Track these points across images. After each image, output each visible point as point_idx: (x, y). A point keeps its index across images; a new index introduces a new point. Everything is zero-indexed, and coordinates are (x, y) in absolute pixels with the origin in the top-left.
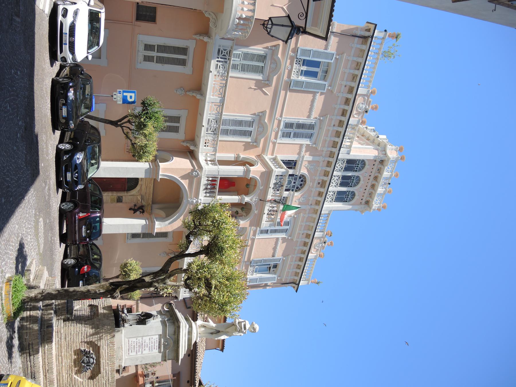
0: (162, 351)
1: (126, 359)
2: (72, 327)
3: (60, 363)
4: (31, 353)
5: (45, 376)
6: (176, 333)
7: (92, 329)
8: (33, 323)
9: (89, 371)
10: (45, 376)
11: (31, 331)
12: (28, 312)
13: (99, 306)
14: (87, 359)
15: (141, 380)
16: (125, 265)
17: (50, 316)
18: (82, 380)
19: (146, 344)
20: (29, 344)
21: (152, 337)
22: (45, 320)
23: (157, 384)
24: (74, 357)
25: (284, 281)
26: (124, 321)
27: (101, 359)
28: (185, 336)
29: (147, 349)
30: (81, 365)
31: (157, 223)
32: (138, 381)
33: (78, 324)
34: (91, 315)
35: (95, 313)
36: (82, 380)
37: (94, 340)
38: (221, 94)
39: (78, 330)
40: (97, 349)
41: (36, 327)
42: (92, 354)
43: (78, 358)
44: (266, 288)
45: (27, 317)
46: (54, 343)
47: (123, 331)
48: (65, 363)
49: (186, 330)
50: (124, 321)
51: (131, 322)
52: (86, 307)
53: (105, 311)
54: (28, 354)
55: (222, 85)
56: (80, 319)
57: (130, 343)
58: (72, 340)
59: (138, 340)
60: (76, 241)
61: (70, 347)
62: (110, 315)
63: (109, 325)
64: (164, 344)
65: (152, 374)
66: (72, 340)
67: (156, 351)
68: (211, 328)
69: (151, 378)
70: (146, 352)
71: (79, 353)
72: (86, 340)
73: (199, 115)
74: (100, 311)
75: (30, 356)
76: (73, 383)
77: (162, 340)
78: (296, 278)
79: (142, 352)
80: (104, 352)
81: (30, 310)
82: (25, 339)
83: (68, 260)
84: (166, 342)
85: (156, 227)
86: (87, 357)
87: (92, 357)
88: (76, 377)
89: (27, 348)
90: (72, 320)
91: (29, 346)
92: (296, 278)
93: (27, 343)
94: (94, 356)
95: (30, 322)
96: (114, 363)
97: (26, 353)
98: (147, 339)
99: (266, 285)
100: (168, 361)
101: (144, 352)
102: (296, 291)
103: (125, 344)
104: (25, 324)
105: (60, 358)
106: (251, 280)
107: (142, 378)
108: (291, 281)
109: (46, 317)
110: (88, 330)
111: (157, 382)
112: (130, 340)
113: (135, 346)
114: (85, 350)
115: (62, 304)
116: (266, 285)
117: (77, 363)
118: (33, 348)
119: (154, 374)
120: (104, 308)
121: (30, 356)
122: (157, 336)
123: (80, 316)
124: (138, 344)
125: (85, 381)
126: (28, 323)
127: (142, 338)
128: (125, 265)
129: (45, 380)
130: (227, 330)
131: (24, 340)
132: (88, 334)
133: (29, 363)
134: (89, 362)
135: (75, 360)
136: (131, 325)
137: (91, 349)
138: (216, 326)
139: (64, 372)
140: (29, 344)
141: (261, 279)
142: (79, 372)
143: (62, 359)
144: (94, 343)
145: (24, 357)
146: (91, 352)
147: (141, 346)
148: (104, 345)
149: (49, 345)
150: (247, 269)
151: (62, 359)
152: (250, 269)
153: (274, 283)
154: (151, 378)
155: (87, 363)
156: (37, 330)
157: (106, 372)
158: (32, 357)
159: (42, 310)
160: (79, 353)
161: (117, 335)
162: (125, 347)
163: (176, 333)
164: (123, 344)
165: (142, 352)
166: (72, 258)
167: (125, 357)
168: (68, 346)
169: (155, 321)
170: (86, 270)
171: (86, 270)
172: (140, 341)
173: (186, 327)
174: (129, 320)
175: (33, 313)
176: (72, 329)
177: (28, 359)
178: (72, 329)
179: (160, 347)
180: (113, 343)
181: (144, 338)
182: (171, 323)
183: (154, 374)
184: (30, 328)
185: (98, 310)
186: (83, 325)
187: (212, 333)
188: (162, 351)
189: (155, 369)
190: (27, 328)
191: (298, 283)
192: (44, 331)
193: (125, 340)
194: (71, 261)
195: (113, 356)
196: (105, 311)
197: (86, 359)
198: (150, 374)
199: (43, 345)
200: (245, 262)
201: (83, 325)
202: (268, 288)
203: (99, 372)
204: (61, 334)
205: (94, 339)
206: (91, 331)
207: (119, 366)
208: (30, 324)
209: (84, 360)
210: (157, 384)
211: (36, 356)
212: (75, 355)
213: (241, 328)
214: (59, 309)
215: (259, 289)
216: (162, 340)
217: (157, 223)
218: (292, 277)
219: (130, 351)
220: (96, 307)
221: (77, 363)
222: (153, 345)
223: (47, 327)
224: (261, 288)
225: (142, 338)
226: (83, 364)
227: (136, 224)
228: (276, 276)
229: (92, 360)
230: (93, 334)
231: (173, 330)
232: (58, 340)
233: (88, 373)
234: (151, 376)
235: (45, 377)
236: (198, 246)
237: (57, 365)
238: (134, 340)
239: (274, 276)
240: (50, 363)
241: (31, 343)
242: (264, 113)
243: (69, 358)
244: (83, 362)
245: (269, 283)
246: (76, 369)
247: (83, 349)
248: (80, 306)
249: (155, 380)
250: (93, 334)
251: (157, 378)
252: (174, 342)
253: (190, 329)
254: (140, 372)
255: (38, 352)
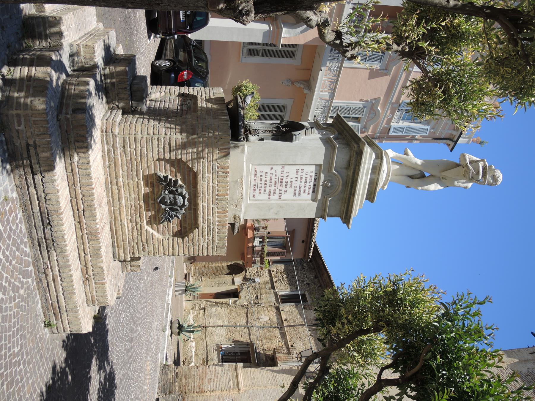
0: (319, 197)
1: (248, 206)
2: (139, 124)
3: (114, 199)
4: (36, 167)
5: (80, 222)
6: (352, 166)
7: (181, 133)
8: (34, 96)
9: (175, 221)
10: (80, 222)
11: (29, 112)
12: (26, 69)
13: (199, 97)
14: (172, 196)
15: (250, 234)
16: (239, 89)
17: (82, 88)
18: (161, 237)
19: (289, 180)
20: (28, 145)
21: (302, 167)
22: (70, 96)
23: (267, 240)
24: (144, 190)
25: (437, 135)
26: (248, 131)
27: (200, 199)
28: (367, 175)
29: (290, 191)
30: (160, 207)
31: (284, 30)
32: (246, 234)
33: (152, 121)
34: (181, 110)
35: (189, 108)
36: (161, 237)
37: (184, 159)
38: (331, 89)
39: (151, 132)
40: (192, 179)
41: (39, 104)
42: (181, 187)
43: (153, 192)
44: (412, 142)
45: (21, 79)
46: (96, 155)
47: (246, 147)
48: (127, 200)
49: (369, 164)
50: (248, 131)
51: (261, 135)
52: (173, 97)
53: (210, 105)
54: (29, 170)
55: (333, 81)
56: (156, 114)
57: (258, 175)
58: (139, 153)
59: (273, 171)
60: (171, 29)
61: (134, 168)
62: (219, 112)
63: (218, 129)
64: (324, 186)
65: (263, 228)
66: (139, 153)
67: (307, 197)
68: (413, 167)
69: (261, 232)
70: (289, 196)
71: (154, 181)
72: (167, 156)
73: (317, 55)
74: (199, 104)
75: (33, 174)
76: (145, 241)
77: (322, 176)
78: (455, 133)
79: (280, 196)
80: (205, 185)
81: (31, 63)
82: (17, 131)
83: (161, 61)
84: (329, 181)
85: (283, 36)
86: (170, 192)
87: (181, 194)
88: (150, 229)
89: (25, 155)
90: (141, 113)
91: (28, 150)
92: (455, 133)
93: (24, 143)
94: (184, 192)
95: (27, 91)
96: (225, 211)
97: (24, 166)
98: (291, 170)
99: (413, 138)
100: (328, 219)
101: (284, 196)
102: (451, 150)
103: (247, 176)
104: (16, 95)
105: (115, 188)
106: (396, 129)
107: (252, 232)
108: (447, 137)
109: (73, 90)
110: (173, 134)
111: (268, 238)
112: (259, 168)
113: (268, 183)
114: (166, 177)
115: (118, 74)
116: (413, 138)
117: (151, 202)
118: (37, 154)
119: (265, 228)
120: (207, 100)
121: (33, 174)
122: (313, 168)
123: (160, 109)
124: (274, 179)
125: (168, 240)
126: (22, 94)
127: (283, 168)
128: (239, 89)
129: (79, 230)
130: (445, 174)
131: (14, 135)
132: (173, 144)
133: (32, 190)
134: (175, 203)
135: (146, 196)
136: (262, 140)
137: (179, 176)
138: (422, 164)
139: (124, 218)
140: (28, 145)
141: (409, 129)
142: (154, 221)
143: (119, 191)
144: (185, 163)
145: (20, 176)
146: (180, 182)
147: (280, 183)
148: (205, 169)
149: (81, 155)
150: (393, 113)
151: (119, 191)
152: (397, 114)
153: (424, 137)
154: (261, 232)
155: (171, 204)
156: (45, 112)
157: (209, 227)
158: (38, 177)
159: (68, 75)
160: (154, 181)
161: (233, 153)
162: (248, 182)
163: (352, 166)
164: (245, 174)
165: (280, 196)
166: (168, 60)
167: (247, 201)
168: (130, 165)
169: (308, 137)
170: (185, 77)
171: (185, 77)
172: (279, 174)
173: (371, 156)
174: (256, 132)
175: (38, 72)
176: (139, 129)
177: (30, 180)
178: (139, 129)
179: (315, 190)
180: (224, 169)
181: (287, 168)
182: (343, 144)
183: (265, 228)
184: (26, 105)
185: (196, 103)
186: (162, 124)
187: (412, 177)
188: (319, 197)
189: (267, 223)
190: (19, 104)
191: (455, 139)
192: (68, 119)
193: (248, 167)
194: (164, 64)
195: (224, 195)
196: (210, 105)
197: (168, 197)
198: (261, 228)
199: (67, 153)
200: (393, 104)
201: (162, 124)
202: (415, 142)
203: (195, 225)
204: (114, 136)
205: (186, 156)
206: (179, 136)
207: (235, 217)
208: (26, 97)
209: (164, 198)
210: (267, 240)
211: (48, 176)
212: (146, 185)
213: (478, 173)
214: (113, 84)
215: (403, 142)
216: (322, 176)
217: (284, 30)
218: (450, 132)
219: (257, 191)
220: (195, 98)
221: (151, 202)
222: (303, 184)
223: (74, 111)
224: (406, 142)
225: (283, 168)
226: (163, 206)
227: (255, 30)
228: (429, 127)
229: (180, 200)
230: (184, 146)
231: (347, 158)
232: (109, 150)
233: (174, 225)
234: (261, 230)
235: (78, 225)
236: (335, 73)
237: (109, 201)
238: (267, 169)
239: (426, 127)
240: (88, 196)
241: (31, 142)
242: (377, 100)
243: (134, 192)
244: (163, 201)
245: (418, 136)
246: (149, 214)
247: (162, 174)
248: (163, 94)
249: (266, 235)
250: (184, 146)
251: (269, 233)
252: (345, 184)
253: (378, 161)
254: (249, 224)
255: (51, 167)
